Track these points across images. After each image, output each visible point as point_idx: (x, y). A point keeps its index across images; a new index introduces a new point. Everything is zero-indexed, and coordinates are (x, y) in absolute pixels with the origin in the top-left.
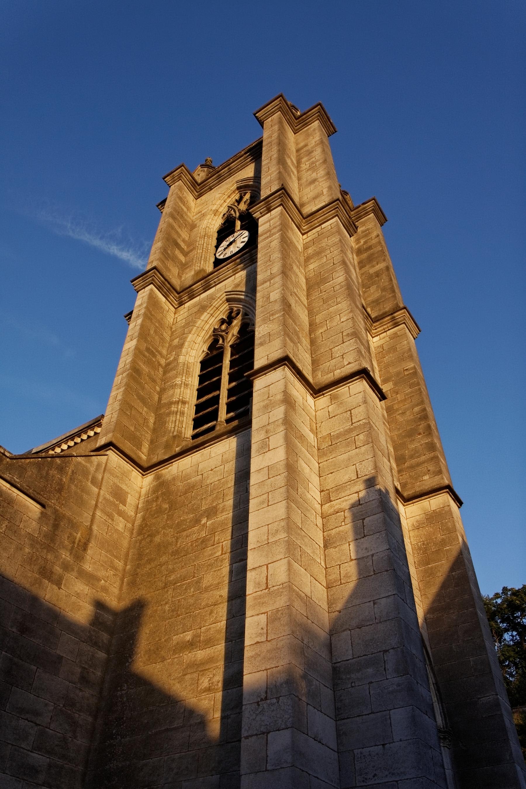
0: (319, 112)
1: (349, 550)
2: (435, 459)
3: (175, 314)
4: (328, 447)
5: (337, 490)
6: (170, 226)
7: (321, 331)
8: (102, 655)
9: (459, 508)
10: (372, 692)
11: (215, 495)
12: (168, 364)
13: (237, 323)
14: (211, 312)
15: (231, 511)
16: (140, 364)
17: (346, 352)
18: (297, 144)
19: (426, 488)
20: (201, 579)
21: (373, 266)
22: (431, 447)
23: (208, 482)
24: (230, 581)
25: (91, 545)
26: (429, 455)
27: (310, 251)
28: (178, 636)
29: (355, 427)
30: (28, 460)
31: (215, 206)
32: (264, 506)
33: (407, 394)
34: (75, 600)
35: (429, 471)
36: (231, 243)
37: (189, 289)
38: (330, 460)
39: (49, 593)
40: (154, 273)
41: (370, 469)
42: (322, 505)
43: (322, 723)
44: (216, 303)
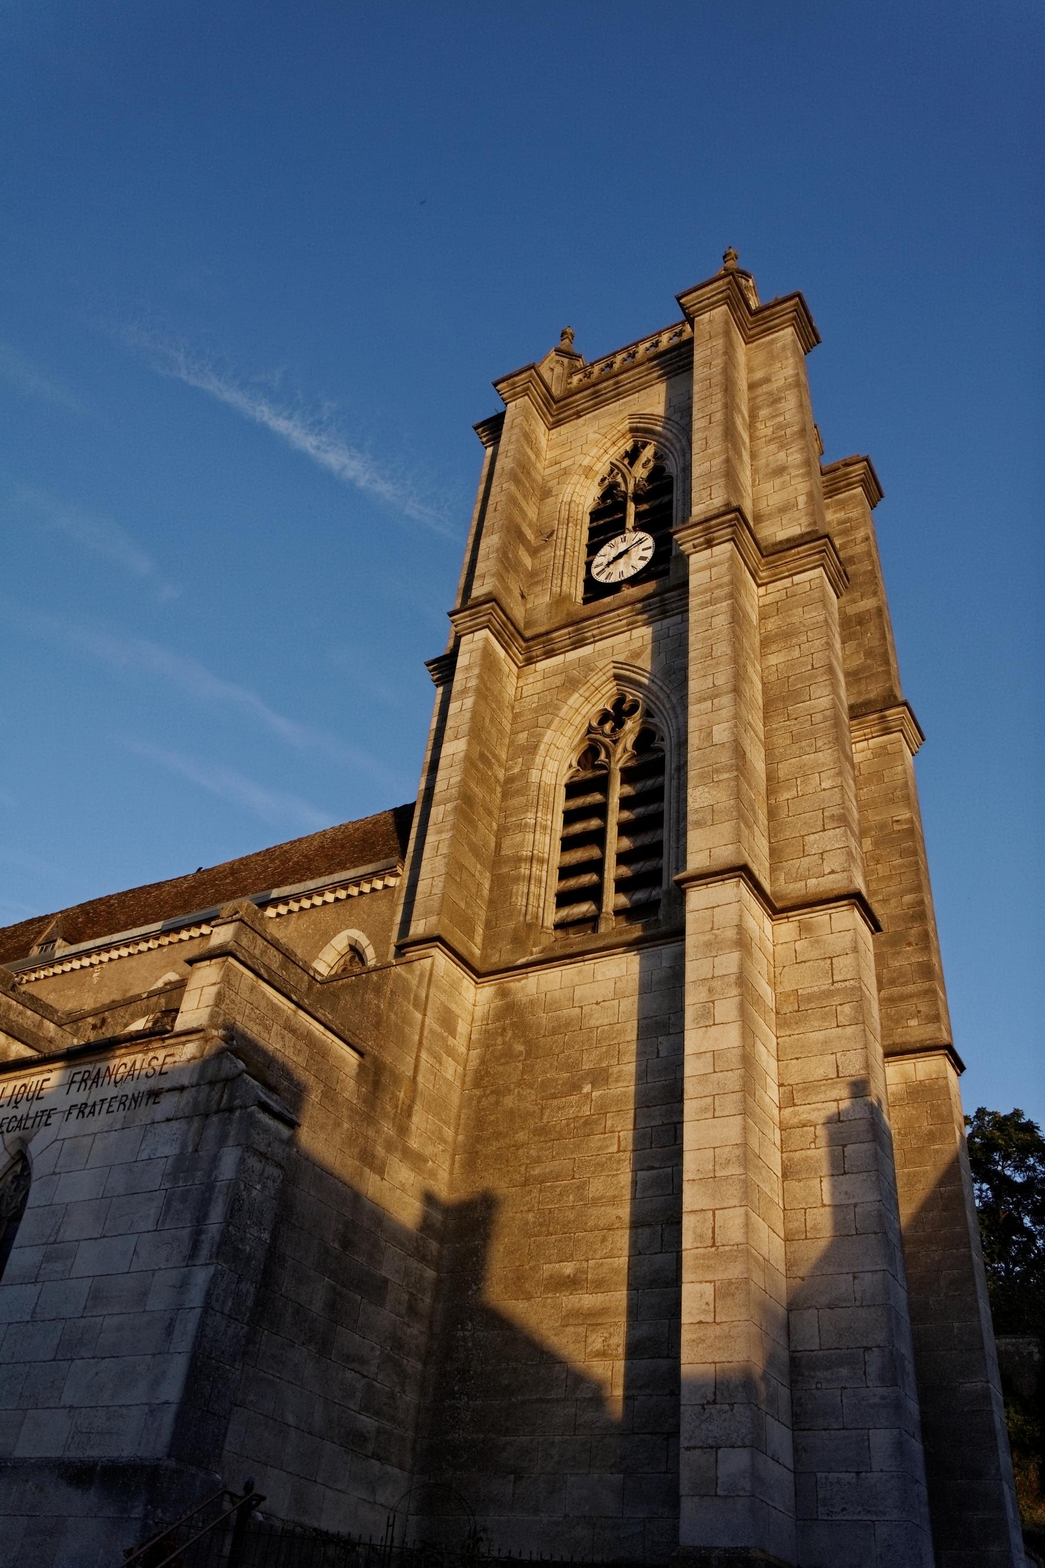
0: (795, 310)
1: (822, 1189)
2: (931, 992)
3: (518, 678)
4: (795, 1011)
5: (805, 1089)
6: (513, 501)
7: (786, 796)
8: (430, 1274)
9: (958, 1075)
10: (845, 1401)
11: (604, 1049)
12: (510, 780)
13: (632, 726)
14: (587, 694)
15: (633, 1083)
16: (472, 786)
17: (828, 849)
18: (750, 370)
19: (913, 1040)
20: (585, 1183)
21: (854, 601)
22: (927, 971)
23: (593, 1023)
24: (633, 1198)
25: (416, 1108)
26: (921, 986)
27: (771, 625)
28: (552, 1266)
29: (838, 990)
30: (340, 982)
31: (588, 458)
32: (707, 1116)
33: (894, 867)
34: (400, 1194)
35: (919, 1012)
36: (620, 556)
37: (545, 638)
38: (796, 1037)
39: (372, 1186)
40: (492, 608)
41: (858, 1067)
42: (780, 1108)
43: (779, 1436)
44: (596, 679)
